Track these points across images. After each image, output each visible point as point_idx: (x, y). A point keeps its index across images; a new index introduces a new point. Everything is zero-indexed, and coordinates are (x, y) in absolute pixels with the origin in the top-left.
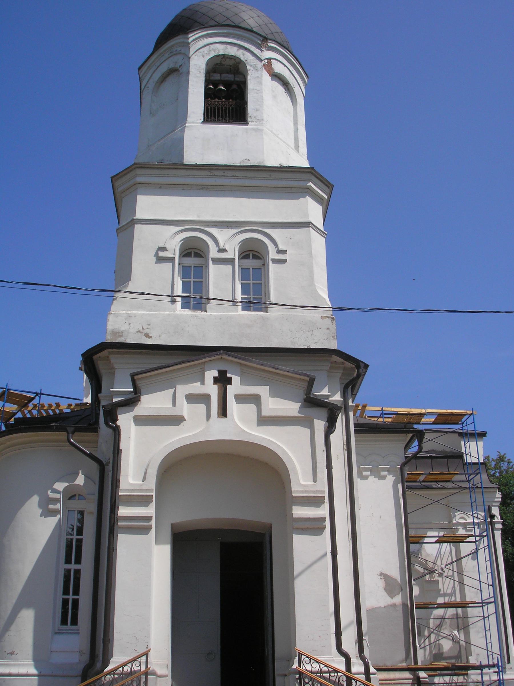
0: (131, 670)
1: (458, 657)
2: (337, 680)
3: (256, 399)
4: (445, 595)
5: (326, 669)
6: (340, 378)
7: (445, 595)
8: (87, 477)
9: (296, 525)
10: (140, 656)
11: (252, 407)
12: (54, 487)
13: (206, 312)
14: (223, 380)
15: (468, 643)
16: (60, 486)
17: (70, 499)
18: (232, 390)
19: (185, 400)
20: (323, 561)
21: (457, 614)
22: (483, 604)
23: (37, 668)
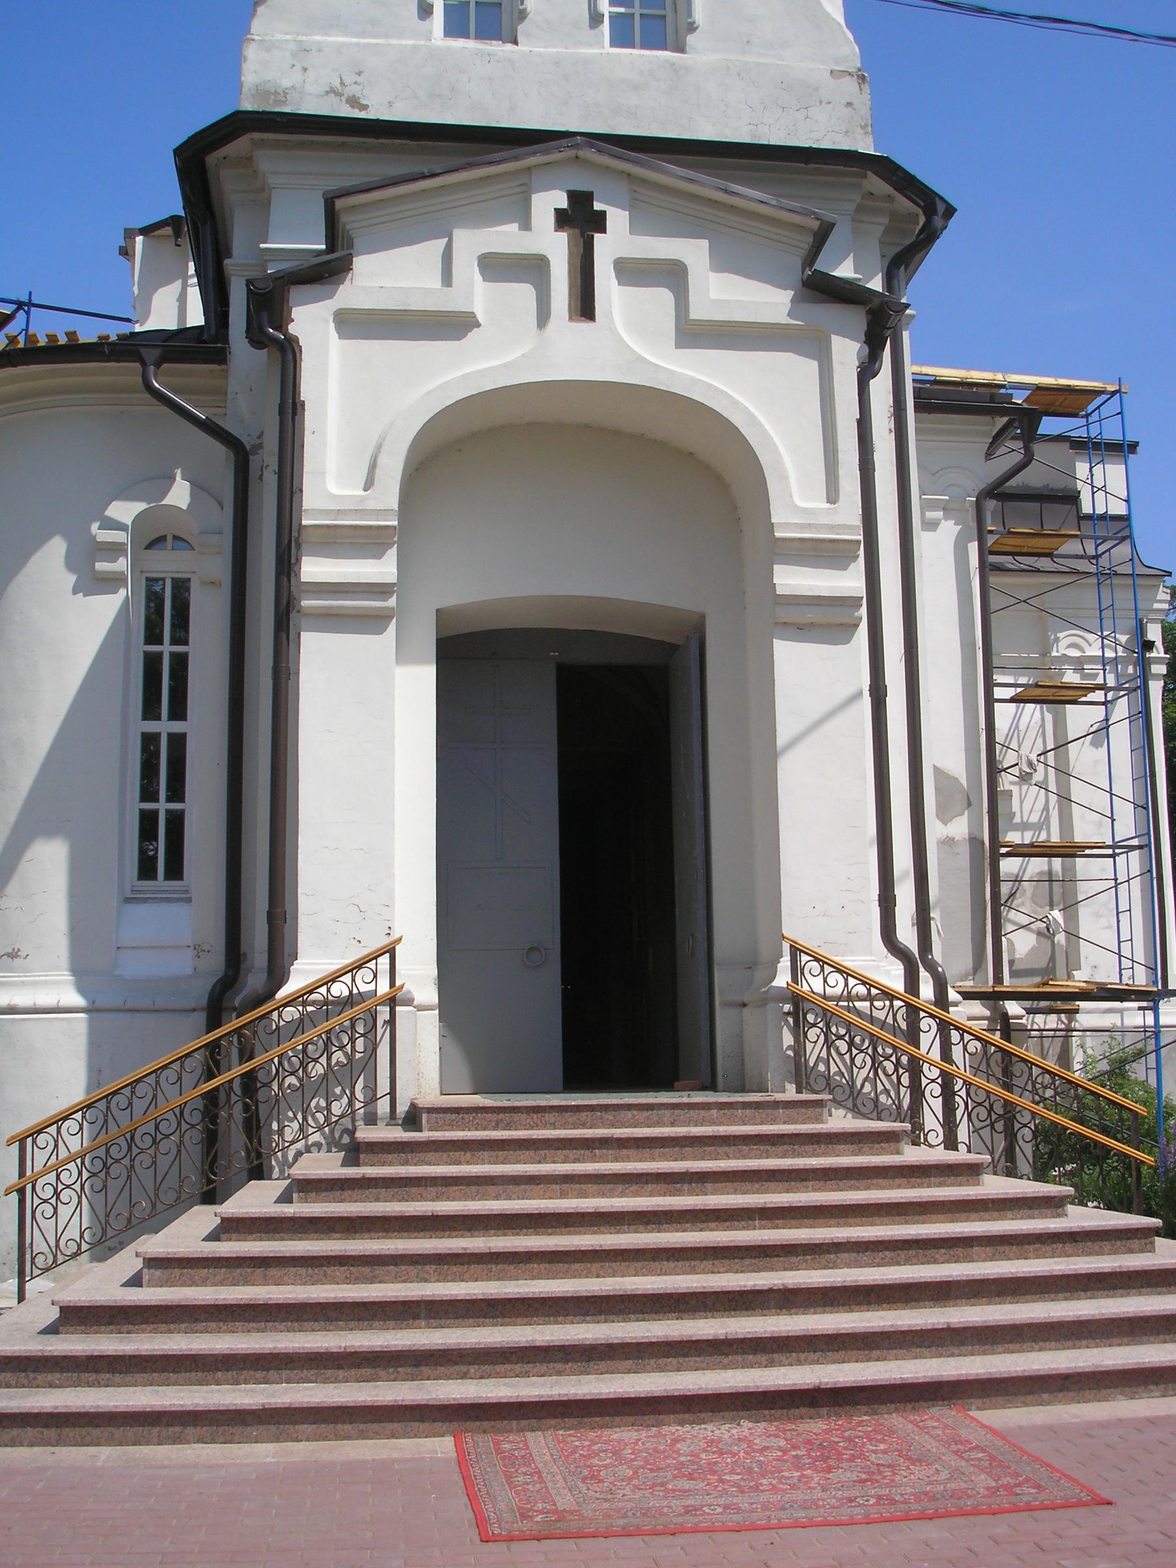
0: (351, 992)
1: (1049, 971)
2: (890, 1020)
3: (672, 275)
4: (1024, 826)
5: (862, 990)
6: (881, 242)
7: (1024, 826)
8: (197, 486)
9: (784, 615)
10: (375, 957)
11: (662, 298)
12: (107, 513)
13: (516, 42)
14: (581, 219)
15: (1073, 936)
16: (125, 511)
17: (149, 546)
18: (607, 248)
19: (477, 269)
20: (854, 709)
21: (1050, 872)
22: (1116, 849)
23: (81, 990)
